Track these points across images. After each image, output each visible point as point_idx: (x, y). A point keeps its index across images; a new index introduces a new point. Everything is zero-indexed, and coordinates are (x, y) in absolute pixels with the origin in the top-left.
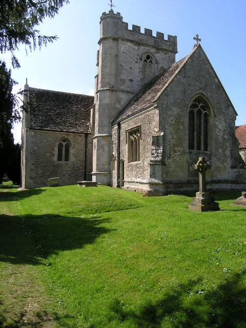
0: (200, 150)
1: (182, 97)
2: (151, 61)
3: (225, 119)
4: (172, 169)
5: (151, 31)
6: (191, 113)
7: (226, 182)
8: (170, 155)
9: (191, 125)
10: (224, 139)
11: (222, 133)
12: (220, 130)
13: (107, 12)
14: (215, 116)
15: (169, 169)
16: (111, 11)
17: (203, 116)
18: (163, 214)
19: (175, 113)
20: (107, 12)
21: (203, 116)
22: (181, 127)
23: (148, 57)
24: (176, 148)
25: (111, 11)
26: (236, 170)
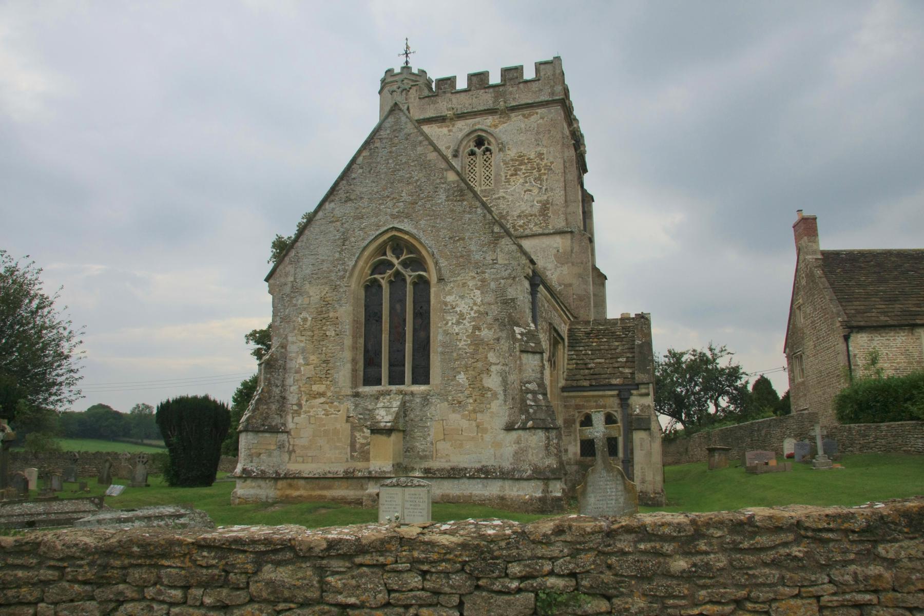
0: (427, 382)
1: (337, 255)
2: (488, 150)
3: (483, 281)
4: (303, 442)
5: (519, 70)
6: (372, 288)
7: (485, 474)
8: (300, 405)
9: (372, 316)
10: (477, 343)
11: (468, 324)
12: (462, 316)
13: (397, 70)
14: (441, 280)
15: (297, 442)
16: (406, 68)
17: (409, 289)
18: (361, 576)
19: (315, 299)
20: (397, 70)
21: (409, 289)
22: (331, 333)
23: (480, 142)
24: (315, 388)
25: (406, 68)
26: (514, 435)
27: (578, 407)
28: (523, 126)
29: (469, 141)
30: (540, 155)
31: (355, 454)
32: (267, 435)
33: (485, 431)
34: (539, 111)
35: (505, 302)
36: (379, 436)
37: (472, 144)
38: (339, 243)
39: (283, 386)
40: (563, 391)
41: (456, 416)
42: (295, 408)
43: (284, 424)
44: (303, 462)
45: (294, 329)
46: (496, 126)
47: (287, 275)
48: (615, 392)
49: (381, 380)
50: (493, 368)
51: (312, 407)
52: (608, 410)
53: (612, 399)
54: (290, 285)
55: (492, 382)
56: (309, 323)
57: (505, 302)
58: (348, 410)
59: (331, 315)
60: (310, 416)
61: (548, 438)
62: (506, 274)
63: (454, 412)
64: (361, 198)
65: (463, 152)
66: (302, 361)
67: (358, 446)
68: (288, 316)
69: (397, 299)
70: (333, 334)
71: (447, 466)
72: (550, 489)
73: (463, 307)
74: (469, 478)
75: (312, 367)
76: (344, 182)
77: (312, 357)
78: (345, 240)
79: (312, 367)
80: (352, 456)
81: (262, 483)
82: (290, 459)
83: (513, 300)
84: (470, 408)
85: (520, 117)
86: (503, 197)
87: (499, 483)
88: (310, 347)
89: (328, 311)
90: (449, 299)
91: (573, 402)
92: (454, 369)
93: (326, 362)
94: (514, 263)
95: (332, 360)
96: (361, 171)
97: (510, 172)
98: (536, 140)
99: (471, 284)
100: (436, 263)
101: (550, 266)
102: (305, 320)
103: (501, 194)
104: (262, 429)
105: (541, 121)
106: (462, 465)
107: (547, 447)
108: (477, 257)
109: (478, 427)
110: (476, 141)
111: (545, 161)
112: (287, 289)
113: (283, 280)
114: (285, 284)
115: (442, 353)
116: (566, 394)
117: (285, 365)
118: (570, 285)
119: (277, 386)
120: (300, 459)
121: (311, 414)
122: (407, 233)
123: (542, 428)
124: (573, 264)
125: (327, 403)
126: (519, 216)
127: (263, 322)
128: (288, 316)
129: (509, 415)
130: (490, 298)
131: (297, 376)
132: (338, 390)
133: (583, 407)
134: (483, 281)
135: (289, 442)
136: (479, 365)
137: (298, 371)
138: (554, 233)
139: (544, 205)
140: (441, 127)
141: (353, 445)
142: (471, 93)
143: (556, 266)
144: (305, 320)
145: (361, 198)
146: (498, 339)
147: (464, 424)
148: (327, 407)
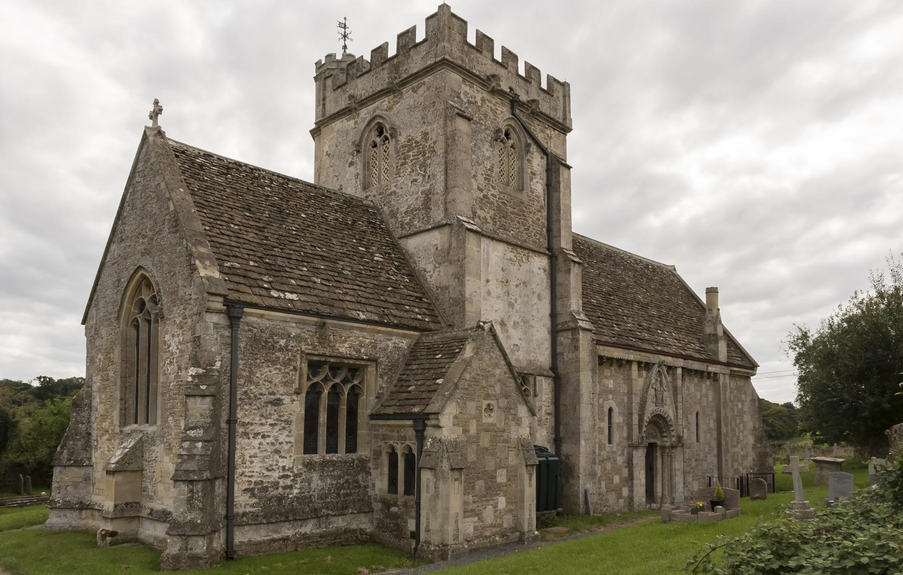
27: (384, 438)
29: (370, 131)
30: (425, 135)
32: (73, 468)
34: (426, 80)
37: (374, 134)
39: (89, 422)
40: (372, 419)
43: (90, 459)
46: (390, 109)
48: (410, 422)
52: (408, 443)
61: (192, 491)
65: (366, 145)
72: (189, 547)
81: (68, 513)
86: (395, 192)
91: (382, 431)
97: (400, 162)
98: (423, 118)
101: (430, 267)
103: (393, 189)
104: (68, 463)
107: (190, 500)
111: (430, 142)
116: (373, 422)
117: (91, 403)
118: (447, 288)
119: (83, 423)
123: (184, 481)
124: (451, 263)
126: (406, 212)
133: (390, 438)
138: (433, 228)
139: (427, 195)
140: (348, 120)
142: (372, 73)
143: (435, 267)
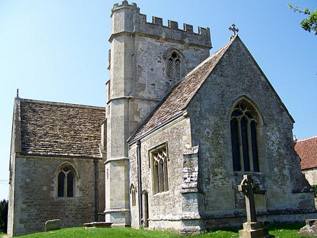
6: (234, 124)
8: (209, 179)
10: (280, 154)
15: (209, 199)
19: (212, 123)
21: (239, 124)
23: (174, 55)
28: (194, 54)
31: (237, 205)
33: (286, 193)
35: (287, 139)
36: (259, 194)
38: (221, 96)
41: (275, 187)
42: (207, 180)
44: (213, 210)
45: (203, 137)
47: (196, 106)
49: (241, 168)
50: (286, 166)
51: (216, 180)
53: (257, 203)
54: (198, 112)
55: (286, 172)
56: (211, 135)
57: (287, 139)
58: (233, 182)
59: (221, 132)
60: (215, 185)
62: (286, 127)
63: (274, 185)
64: (228, 77)
66: (208, 155)
67: (238, 200)
68: (199, 129)
69: (245, 130)
70: (223, 142)
71: (274, 209)
73: (273, 138)
74: (283, 214)
75: (214, 159)
76: (219, 66)
77: (213, 154)
78: (223, 95)
79: (214, 159)
80: (236, 206)
82: (205, 209)
83: (290, 138)
84: (280, 183)
85: (193, 50)
87: (293, 216)
88: (212, 148)
89: (219, 131)
90: (268, 134)
92: (272, 165)
93: (220, 157)
94: (289, 123)
95: (223, 156)
96: (226, 63)
99: (275, 128)
100: (263, 117)
102: (208, 133)
105: (201, 54)
106: (280, 209)
108: (276, 117)
109: (283, 191)
110: (172, 54)
112: (197, 114)
113: (194, 109)
114: (196, 111)
115: (268, 158)
120: (211, 209)
121: (215, 184)
122: (249, 99)
125: (223, 178)
127: (294, 124)
128: (199, 129)
129: (294, 187)
130: (282, 136)
131: (207, 163)
132: (227, 172)
134: (279, 128)
135: (205, 199)
136: (281, 164)
137: (207, 161)
141: (236, 200)
144: (208, 133)
145: (228, 77)
146: (286, 154)
147: (279, 190)
148: (223, 180)
